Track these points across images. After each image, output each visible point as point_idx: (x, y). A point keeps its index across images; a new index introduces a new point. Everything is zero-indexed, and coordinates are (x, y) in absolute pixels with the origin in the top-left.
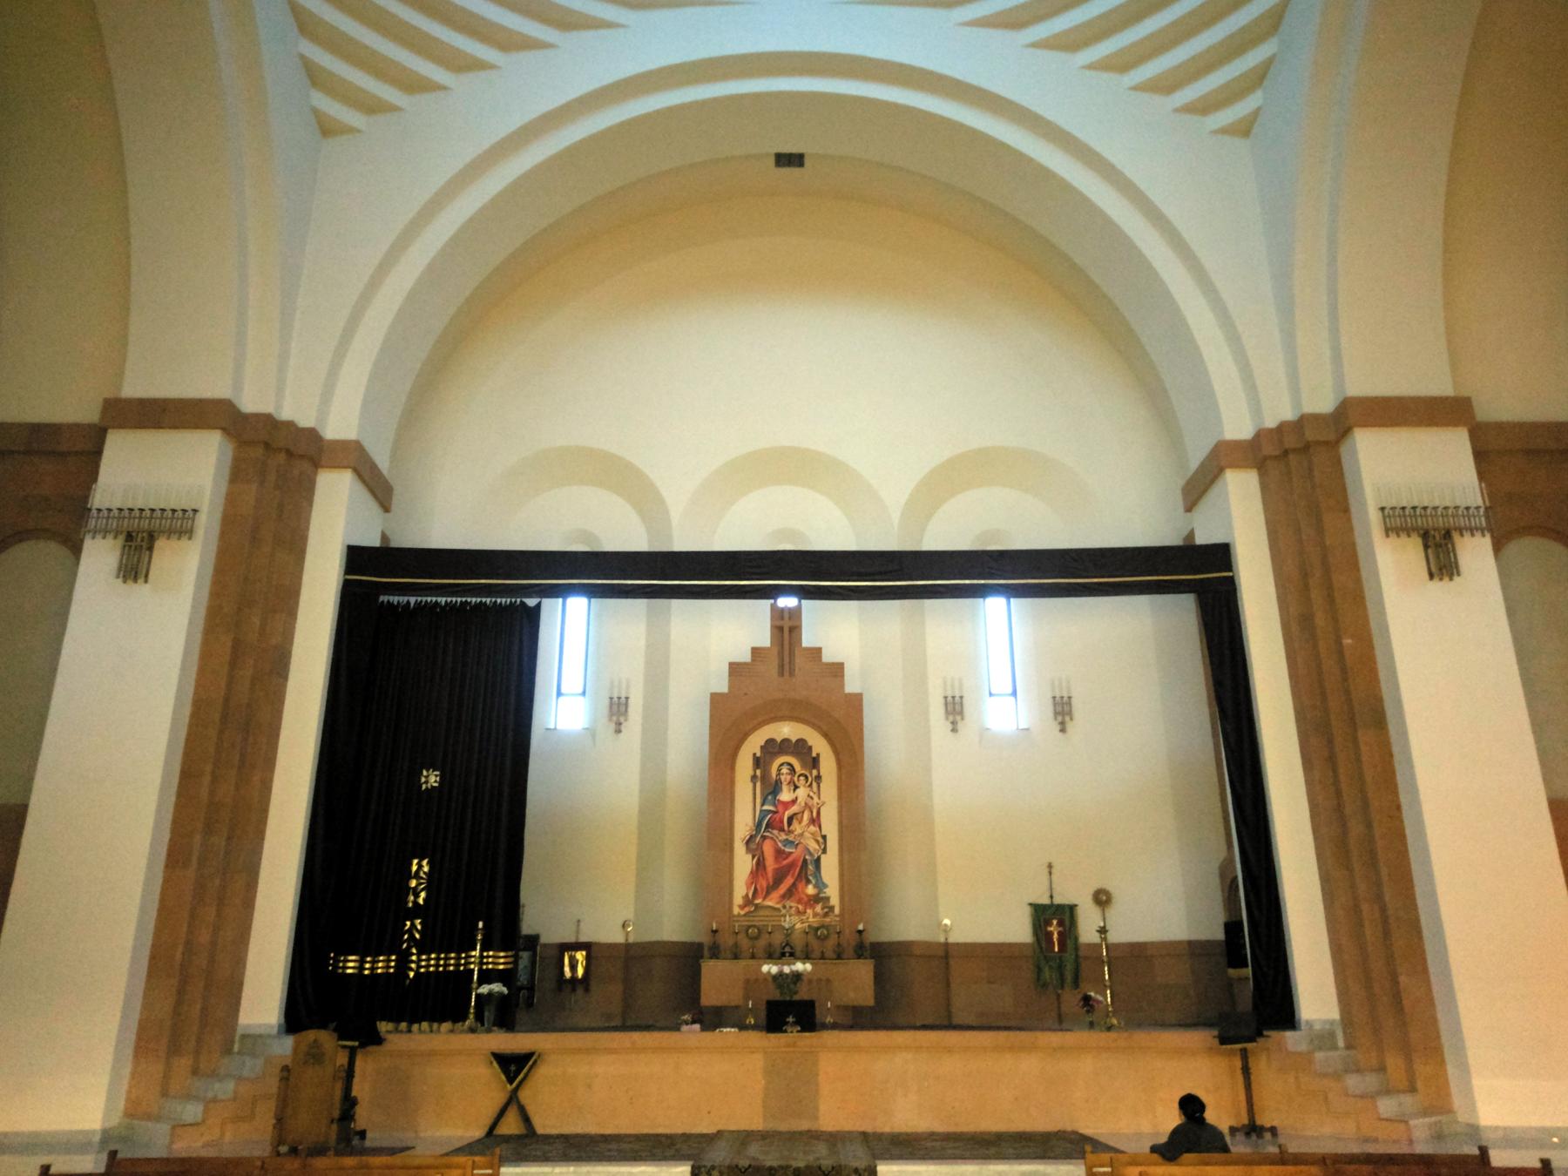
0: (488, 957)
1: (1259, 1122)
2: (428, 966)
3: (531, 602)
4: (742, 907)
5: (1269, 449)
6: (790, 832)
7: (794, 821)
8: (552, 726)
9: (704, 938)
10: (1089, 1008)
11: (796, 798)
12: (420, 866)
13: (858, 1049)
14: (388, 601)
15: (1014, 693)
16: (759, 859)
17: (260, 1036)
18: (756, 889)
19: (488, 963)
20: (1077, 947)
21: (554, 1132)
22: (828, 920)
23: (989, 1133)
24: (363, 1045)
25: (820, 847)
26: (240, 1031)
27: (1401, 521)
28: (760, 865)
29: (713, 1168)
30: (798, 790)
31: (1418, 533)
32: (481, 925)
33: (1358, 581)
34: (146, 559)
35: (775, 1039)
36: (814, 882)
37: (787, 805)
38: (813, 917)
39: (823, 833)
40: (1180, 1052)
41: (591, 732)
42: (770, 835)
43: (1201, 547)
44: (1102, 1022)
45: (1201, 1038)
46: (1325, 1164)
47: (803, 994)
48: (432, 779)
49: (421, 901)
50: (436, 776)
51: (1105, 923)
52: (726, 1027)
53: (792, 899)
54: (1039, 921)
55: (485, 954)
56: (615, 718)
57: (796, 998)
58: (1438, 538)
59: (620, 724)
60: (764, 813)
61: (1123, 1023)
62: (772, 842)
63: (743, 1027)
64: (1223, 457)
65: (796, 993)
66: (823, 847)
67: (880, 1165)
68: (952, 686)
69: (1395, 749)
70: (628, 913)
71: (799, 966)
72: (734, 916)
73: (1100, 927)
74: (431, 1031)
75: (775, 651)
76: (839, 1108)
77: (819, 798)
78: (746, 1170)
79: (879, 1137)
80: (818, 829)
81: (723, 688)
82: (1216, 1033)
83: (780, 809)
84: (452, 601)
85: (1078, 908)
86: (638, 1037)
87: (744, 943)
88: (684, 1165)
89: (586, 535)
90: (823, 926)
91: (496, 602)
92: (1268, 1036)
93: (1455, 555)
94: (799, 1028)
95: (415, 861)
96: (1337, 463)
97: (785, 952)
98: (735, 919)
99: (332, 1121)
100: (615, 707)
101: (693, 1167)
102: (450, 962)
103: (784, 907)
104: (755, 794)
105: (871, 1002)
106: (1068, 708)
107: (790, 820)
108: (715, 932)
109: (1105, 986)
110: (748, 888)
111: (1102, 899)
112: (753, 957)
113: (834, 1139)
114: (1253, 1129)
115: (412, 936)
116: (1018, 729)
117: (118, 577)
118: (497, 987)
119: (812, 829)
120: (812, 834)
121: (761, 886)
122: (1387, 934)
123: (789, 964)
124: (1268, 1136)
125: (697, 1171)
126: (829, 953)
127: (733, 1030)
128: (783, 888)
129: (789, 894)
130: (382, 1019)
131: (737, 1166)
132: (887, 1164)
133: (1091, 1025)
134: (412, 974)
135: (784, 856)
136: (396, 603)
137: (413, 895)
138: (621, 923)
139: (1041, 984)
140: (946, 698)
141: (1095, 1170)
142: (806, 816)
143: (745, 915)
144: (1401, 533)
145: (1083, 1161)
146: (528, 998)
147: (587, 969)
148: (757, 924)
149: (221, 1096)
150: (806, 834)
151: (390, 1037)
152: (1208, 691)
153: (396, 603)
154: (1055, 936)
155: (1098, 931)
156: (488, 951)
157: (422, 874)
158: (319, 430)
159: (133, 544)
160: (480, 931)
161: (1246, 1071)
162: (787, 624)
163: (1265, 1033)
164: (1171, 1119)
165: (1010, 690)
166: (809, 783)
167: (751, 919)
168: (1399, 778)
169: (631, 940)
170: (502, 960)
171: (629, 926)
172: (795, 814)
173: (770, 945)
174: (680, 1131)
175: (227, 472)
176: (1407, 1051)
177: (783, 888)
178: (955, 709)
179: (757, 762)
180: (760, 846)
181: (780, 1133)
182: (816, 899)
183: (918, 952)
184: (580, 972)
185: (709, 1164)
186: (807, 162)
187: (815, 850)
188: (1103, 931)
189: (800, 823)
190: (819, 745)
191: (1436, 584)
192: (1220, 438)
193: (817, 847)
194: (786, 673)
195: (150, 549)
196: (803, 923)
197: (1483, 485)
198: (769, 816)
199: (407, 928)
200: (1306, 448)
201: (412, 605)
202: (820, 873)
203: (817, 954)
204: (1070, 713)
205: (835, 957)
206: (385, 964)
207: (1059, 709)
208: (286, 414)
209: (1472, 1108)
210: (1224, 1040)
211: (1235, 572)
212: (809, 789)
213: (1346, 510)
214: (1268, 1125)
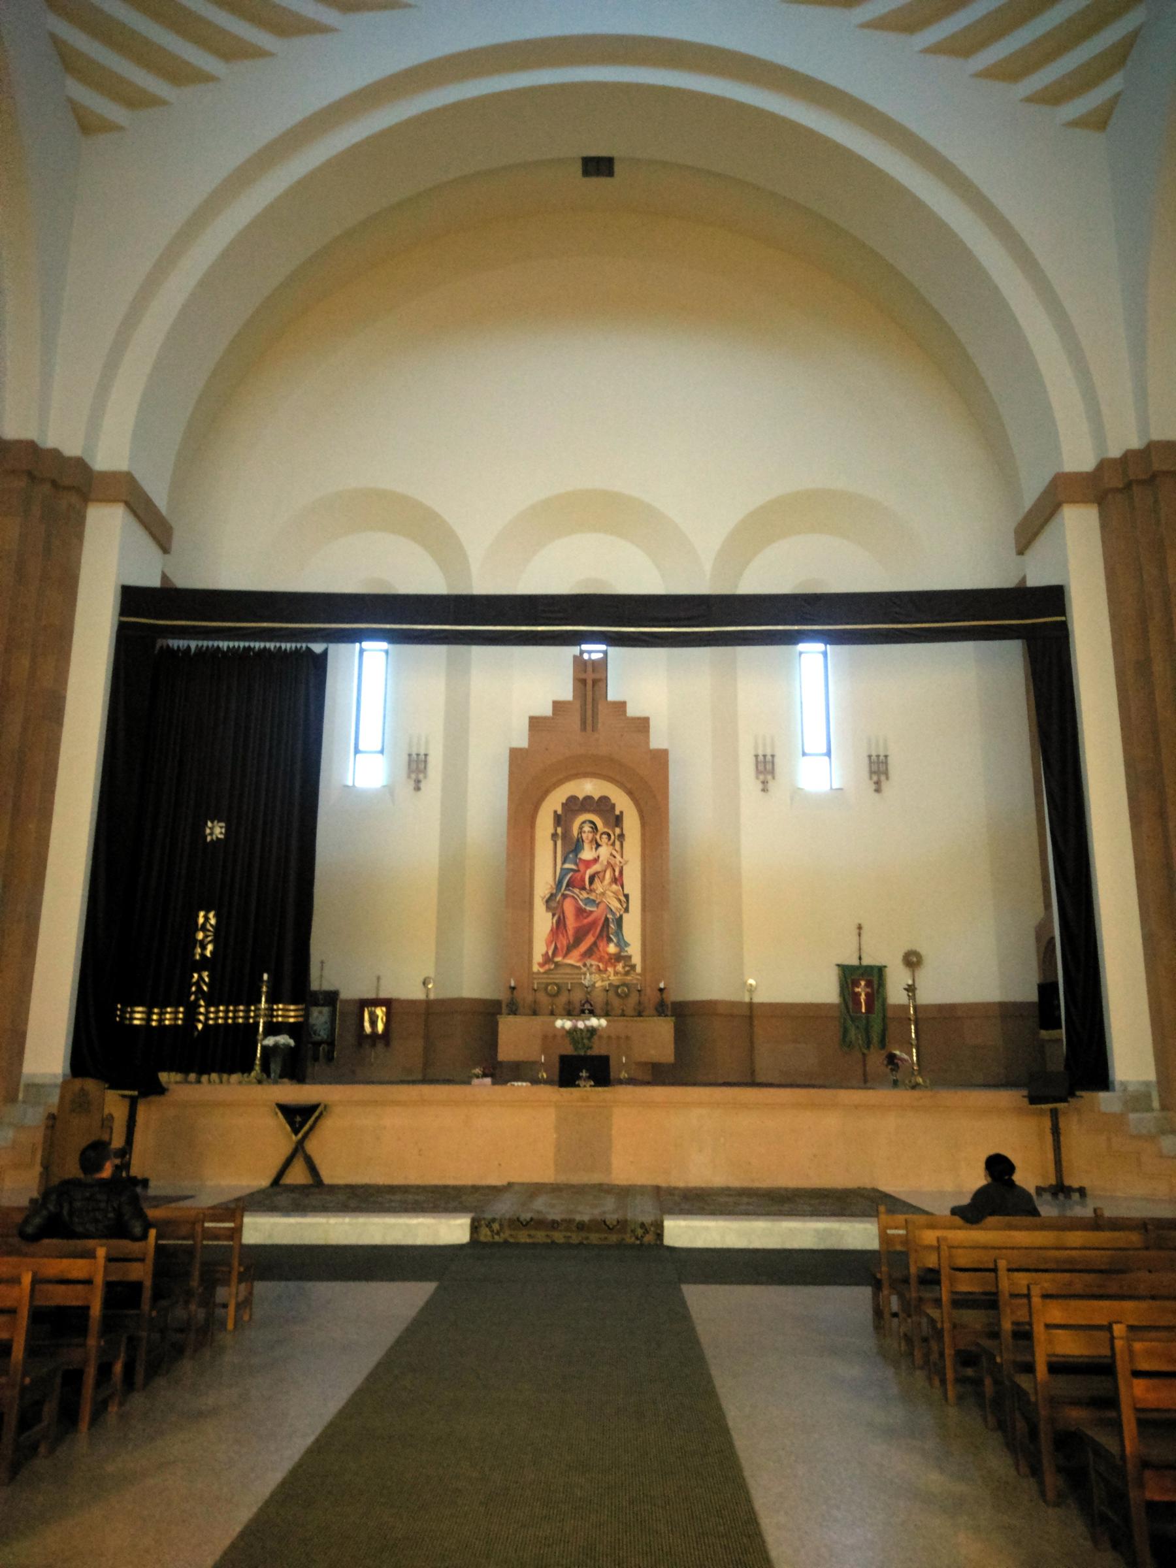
0: (278, 1010)
1: (1069, 1181)
2: (216, 1018)
3: (317, 648)
4: (541, 965)
6: (591, 891)
7: (596, 880)
8: (350, 783)
9: (502, 995)
10: (893, 1067)
11: (598, 857)
12: (207, 919)
15: (829, 754)
16: (559, 918)
17: (43, 1086)
18: (556, 948)
19: (278, 1016)
21: (341, 1182)
22: (629, 978)
23: (786, 1189)
24: (145, 1094)
25: (622, 906)
26: (23, 1081)
28: (560, 924)
29: (494, 1220)
30: (600, 849)
32: (265, 977)
35: (566, 1092)
37: (588, 864)
38: (614, 975)
39: (626, 892)
41: (390, 789)
42: (572, 894)
43: (1031, 588)
44: (907, 1082)
46: (1146, 1230)
47: (598, 1049)
48: (216, 830)
49: (208, 954)
50: (221, 827)
51: (914, 980)
53: (593, 957)
54: (847, 982)
56: (413, 776)
57: (589, 1053)
60: (565, 872)
61: (928, 1081)
63: (535, 1081)
65: (591, 1048)
66: (625, 905)
67: (668, 1219)
68: (764, 745)
70: (430, 972)
71: (594, 1022)
72: (534, 973)
73: (909, 985)
74: (221, 1082)
75: (578, 705)
76: (632, 1162)
77: (622, 857)
78: (528, 1223)
79: (671, 1191)
80: (620, 888)
81: (522, 742)
82: (1025, 1093)
83: (582, 868)
85: (887, 969)
87: (542, 998)
88: (464, 1217)
90: (624, 984)
92: (1081, 1097)
94: (592, 1083)
95: (202, 914)
98: (535, 976)
101: (473, 1221)
102: (239, 1014)
103: (585, 965)
106: (884, 768)
107: (592, 879)
108: (514, 988)
110: (548, 946)
111: (912, 960)
113: (625, 1193)
114: (1060, 1190)
115: (200, 989)
116: (831, 788)
118: (284, 1040)
119: (615, 887)
120: (614, 893)
121: (562, 944)
124: (1076, 1196)
125: (476, 1224)
126: (629, 1011)
127: (524, 1084)
128: (583, 947)
129: (589, 953)
130: (164, 1070)
132: (673, 1219)
133: (895, 1084)
134: (200, 1026)
135: (585, 915)
136: (176, 648)
137: (200, 947)
138: (422, 979)
141: (889, 1232)
142: (608, 875)
143: (545, 973)
145: (876, 1219)
146: (328, 1051)
147: (387, 1025)
148: (557, 981)
150: (609, 893)
151: (172, 1087)
152: (1030, 731)
153: (176, 648)
154: (863, 998)
156: (277, 1003)
157: (208, 927)
158: (87, 460)
160: (265, 983)
161: (1056, 1131)
162: (590, 677)
163: (1078, 1093)
164: (977, 1179)
165: (825, 750)
167: (551, 976)
169: (432, 996)
170: (292, 1014)
171: (429, 983)
172: (597, 873)
173: (569, 1003)
177: (583, 947)
178: (766, 767)
179: (558, 819)
180: (561, 904)
181: (573, 1186)
182: (618, 958)
184: (380, 1027)
186: (617, 168)
187: (617, 908)
188: (911, 989)
190: (622, 802)
192: (1057, 470)
193: (619, 906)
194: (589, 728)
196: (603, 981)
200: (1152, 480)
204: (886, 773)
205: (636, 1014)
207: (874, 768)
208: (50, 441)
210: (1033, 1100)
212: (612, 847)
214: (1076, 1185)
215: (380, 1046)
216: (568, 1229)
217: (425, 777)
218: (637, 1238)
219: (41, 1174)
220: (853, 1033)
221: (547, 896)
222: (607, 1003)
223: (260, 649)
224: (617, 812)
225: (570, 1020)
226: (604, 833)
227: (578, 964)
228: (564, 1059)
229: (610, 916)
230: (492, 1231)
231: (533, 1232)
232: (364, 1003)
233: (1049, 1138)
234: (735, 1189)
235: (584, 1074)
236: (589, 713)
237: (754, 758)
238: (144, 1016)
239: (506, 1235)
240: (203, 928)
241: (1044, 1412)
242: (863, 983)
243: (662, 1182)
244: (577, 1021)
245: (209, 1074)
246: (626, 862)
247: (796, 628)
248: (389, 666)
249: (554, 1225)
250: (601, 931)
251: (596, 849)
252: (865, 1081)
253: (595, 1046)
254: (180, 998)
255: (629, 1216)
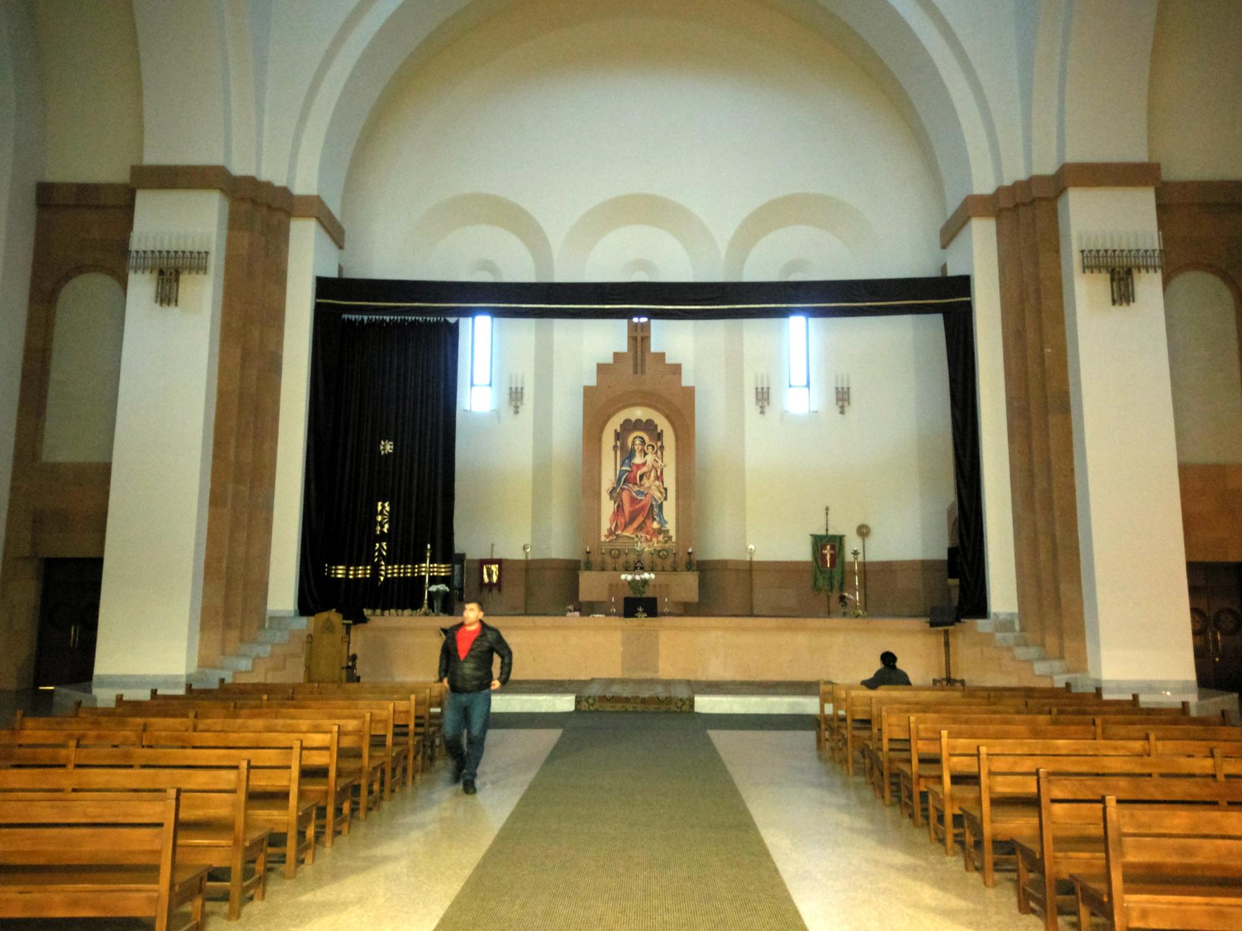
0: (434, 567)
1: (953, 676)
2: (393, 573)
3: (452, 320)
4: (607, 537)
5: (1005, 203)
6: (641, 485)
7: (644, 477)
8: (468, 409)
9: (581, 557)
11: (646, 461)
12: (383, 507)
13: (685, 628)
14: (348, 318)
15: (808, 385)
18: (617, 523)
19: (433, 572)
20: (843, 562)
22: (667, 545)
24: (355, 623)
26: (268, 614)
27: (1095, 261)
28: (620, 508)
29: (589, 697)
30: (647, 456)
31: (1108, 269)
32: (429, 546)
33: (1061, 306)
34: (175, 288)
36: (658, 519)
37: (639, 467)
39: (665, 486)
40: (909, 632)
41: (497, 413)
44: (852, 613)
45: (919, 624)
47: (649, 593)
48: (388, 447)
49: (385, 530)
50: (391, 445)
52: (596, 614)
55: (431, 566)
57: (645, 596)
58: (1121, 274)
59: (518, 407)
62: (628, 493)
63: (608, 614)
64: (973, 207)
66: (664, 495)
69: (1075, 431)
70: (528, 541)
71: (646, 576)
72: (602, 542)
74: (397, 615)
75: (631, 354)
77: (662, 461)
78: (610, 699)
79: (698, 683)
82: (928, 620)
83: (634, 469)
84: (394, 319)
85: (846, 538)
86: (539, 620)
87: (608, 559)
89: (487, 266)
91: (426, 320)
92: (964, 622)
93: (1133, 289)
94: (646, 615)
95: (380, 504)
96: (1055, 212)
97: (638, 567)
99: (342, 668)
100: (514, 396)
101: (576, 697)
104: (616, 464)
105: (696, 600)
107: (641, 477)
108: (588, 553)
109: (855, 589)
110: (611, 524)
111: (863, 531)
112: (615, 569)
113: (668, 683)
115: (381, 554)
116: (809, 411)
117: (156, 302)
119: (657, 483)
122: (1055, 556)
123: (639, 574)
124: (958, 685)
127: (601, 616)
128: (635, 525)
129: (640, 528)
131: (605, 697)
133: (845, 614)
134: (382, 578)
136: (353, 319)
139: (815, 587)
140: (757, 389)
142: (653, 474)
143: (610, 542)
144: (1102, 269)
147: (499, 577)
149: (262, 655)
150: (653, 487)
154: (828, 556)
155: (853, 553)
157: (385, 512)
159: (165, 278)
161: (947, 644)
163: (962, 620)
164: (878, 665)
165: (805, 383)
166: (655, 451)
168: (1075, 449)
169: (530, 558)
170: (443, 570)
174: (567, 678)
175: (225, 225)
176: (1060, 633)
177: (635, 525)
178: (763, 397)
179: (618, 436)
180: (620, 495)
182: (660, 531)
183: (730, 567)
184: (495, 578)
185: (587, 696)
187: (659, 498)
189: (648, 479)
190: (662, 424)
191: (1117, 307)
192: (969, 193)
193: (661, 496)
195: (177, 280)
197: (1160, 233)
198: (627, 474)
199: (377, 548)
201: (365, 321)
202: (662, 513)
203: (660, 568)
204: (848, 400)
206: (363, 572)
208: (265, 175)
209: (1099, 671)
210: (932, 624)
211: (972, 297)
212: (655, 455)
213: (1057, 251)
214: (959, 678)
215: (495, 591)
216: (636, 703)
217: (522, 404)
218: (678, 708)
219: (305, 671)
220: (821, 582)
221: (610, 490)
222: (653, 562)
223: (412, 322)
224: (659, 431)
225: (631, 574)
226: (650, 445)
227: (632, 536)
228: (627, 600)
229: (654, 503)
230: (589, 704)
231: (614, 705)
232: (484, 562)
233: (943, 650)
234: (738, 682)
235: (640, 609)
236: (639, 362)
237: (755, 390)
238: (344, 572)
239: (597, 706)
240: (381, 513)
241: (886, 765)
242: (828, 547)
243: (691, 677)
244: (635, 575)
245: (390, 610)
246: (665, 466)
247: (784, 306)
248: (494, 325)
249: (627, 700)
250: (648, 513)
251: (644, 456)
252: (829, 614)
253: (646, 592)
254: (368, 560)
255: (673, 695)
